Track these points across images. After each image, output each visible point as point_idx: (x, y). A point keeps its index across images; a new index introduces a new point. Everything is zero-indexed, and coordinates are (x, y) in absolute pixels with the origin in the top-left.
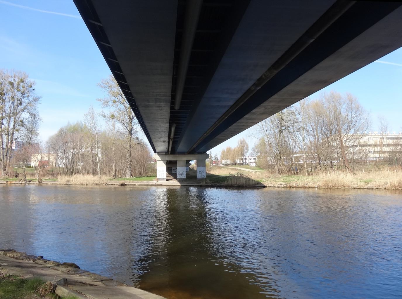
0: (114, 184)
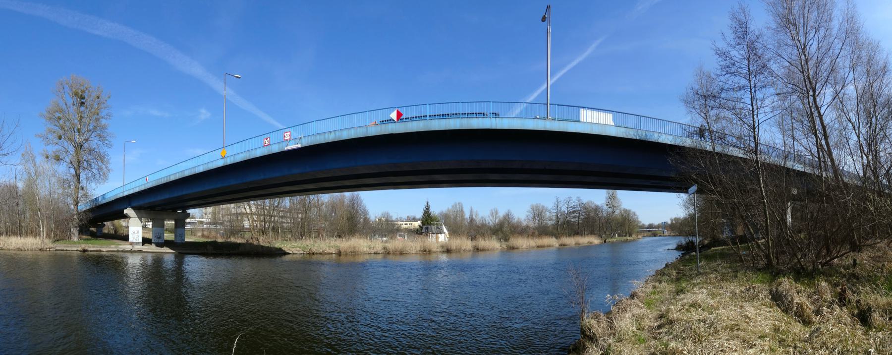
0: (65, 249)
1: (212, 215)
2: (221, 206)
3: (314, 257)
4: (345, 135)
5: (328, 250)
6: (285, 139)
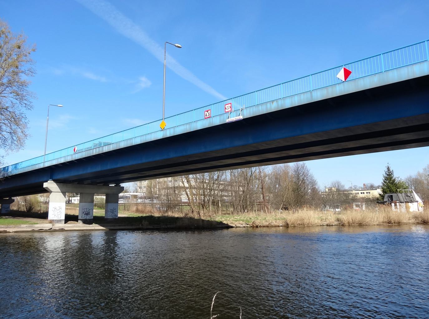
1: (147, 189)
2: (157, 180)
3: (259, 230)
4: (288, 104)
5: (274, 223)
6: (226, 110)
